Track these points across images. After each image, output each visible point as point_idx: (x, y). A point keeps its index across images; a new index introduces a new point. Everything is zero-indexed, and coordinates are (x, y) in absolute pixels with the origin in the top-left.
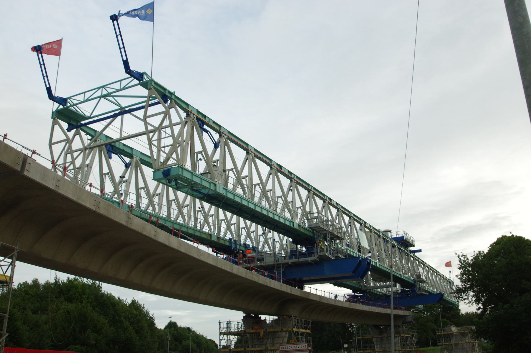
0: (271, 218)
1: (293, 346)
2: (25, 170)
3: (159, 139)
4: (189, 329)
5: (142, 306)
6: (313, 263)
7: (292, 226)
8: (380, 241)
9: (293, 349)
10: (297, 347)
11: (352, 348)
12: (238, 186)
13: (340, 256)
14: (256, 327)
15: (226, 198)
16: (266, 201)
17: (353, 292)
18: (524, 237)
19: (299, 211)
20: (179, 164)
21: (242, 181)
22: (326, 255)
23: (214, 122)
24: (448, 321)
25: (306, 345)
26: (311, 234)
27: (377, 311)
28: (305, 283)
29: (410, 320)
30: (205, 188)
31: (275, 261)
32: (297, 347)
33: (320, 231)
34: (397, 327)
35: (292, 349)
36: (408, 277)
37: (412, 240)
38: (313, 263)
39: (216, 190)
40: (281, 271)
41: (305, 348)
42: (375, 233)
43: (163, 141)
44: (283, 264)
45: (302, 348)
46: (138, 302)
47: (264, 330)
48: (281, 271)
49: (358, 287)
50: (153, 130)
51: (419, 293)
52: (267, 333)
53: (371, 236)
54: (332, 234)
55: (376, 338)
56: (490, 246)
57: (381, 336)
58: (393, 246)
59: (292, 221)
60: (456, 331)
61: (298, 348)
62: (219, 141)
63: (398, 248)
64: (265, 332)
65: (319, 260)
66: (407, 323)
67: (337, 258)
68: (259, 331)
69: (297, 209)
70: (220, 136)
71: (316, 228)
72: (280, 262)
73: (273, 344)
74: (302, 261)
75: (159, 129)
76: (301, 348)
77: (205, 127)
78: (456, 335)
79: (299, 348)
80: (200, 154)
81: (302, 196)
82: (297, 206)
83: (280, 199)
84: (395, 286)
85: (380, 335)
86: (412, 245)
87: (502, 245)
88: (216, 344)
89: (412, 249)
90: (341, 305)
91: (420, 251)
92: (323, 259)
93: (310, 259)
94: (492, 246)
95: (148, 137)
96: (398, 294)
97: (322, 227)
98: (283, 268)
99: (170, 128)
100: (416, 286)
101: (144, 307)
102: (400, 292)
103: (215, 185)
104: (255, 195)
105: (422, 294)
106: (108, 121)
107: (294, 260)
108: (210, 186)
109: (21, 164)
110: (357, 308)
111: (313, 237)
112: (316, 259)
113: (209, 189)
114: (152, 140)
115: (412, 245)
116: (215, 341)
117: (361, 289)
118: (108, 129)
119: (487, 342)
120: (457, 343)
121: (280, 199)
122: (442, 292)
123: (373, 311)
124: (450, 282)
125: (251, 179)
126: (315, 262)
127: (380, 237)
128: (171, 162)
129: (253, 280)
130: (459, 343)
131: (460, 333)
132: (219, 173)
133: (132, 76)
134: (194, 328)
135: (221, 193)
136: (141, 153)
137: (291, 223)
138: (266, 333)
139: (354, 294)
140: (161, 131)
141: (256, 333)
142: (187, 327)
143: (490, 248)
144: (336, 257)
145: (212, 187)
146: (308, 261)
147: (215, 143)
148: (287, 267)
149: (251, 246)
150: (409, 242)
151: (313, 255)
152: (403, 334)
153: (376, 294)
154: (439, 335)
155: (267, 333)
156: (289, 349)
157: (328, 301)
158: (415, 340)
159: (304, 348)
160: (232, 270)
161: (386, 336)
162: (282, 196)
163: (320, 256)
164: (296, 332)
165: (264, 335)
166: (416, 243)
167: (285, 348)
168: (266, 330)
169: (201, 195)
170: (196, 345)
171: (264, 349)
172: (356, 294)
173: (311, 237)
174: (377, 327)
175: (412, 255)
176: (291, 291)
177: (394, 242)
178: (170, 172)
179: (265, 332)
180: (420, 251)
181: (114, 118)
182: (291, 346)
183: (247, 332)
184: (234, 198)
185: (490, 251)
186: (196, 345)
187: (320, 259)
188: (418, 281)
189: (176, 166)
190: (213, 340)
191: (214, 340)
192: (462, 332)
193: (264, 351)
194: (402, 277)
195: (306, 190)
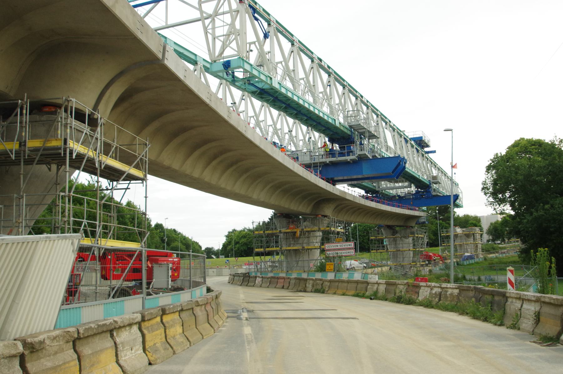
0: (316, 114)
1: (339, 245)
2: (165, 59)
3: (214, 28)
4: (175, 230)
5: (138, 207)
6: (352, 162)
7: (334, 123)
9: (339, 247)
10: (343, 246)
13: (377, 155)
14: (292, 226)
17: (365, 193)
18: (541, 139)
20: (240, 55)
22: (365, 154)
23: (264, 10)
24: (444, 222)
25: (352, 243)
26: (349, 133)
27: (397, 212)
28: (337, 183)
29: (423, 220)
30: (262, 81)
31: (311, 159)
32: (343, 246)
33: (358, 129)
34: (411, 228)
35: (337, 248)
36: (424, 178)
37: (428, 141)
38: (352, 162)
39: (272, 84)
40: (318, 171)
41: (350, 247)
42: (398, 132)
43: (217, 30)
44: (321, 163)
45: (348, 247)
46: (133, 203)
47: (301, 230)
48: (318, 171)
49: (372, 187)
50: (199, 19)
51: (434, 194)
52: (304, 232)
53: (394, 135)
54: (369, 132)
55: (389, 238)
56: (507, 148)
57: (394, 236)
58: (412, 146)
60: (461, 232)
61: (344, 247)
63: (416, 149)
64: (301, 232)
65: (357, 159)
66: (420, 224)
67: (374, 157)
68: (295, 230)
70: (269, 25)
71: (355, 126)
72: (317, 161)
73: (308, 244)
74: (340, 161)
75: (213, 17)
76: (347, 247)
77: (256, 15)
78: (461, 237)
79: (345, 247)
84: (410, 187)
85: (392, 235)
86: (428, 146)
87: (521, 147)
88: (200, 245)
89: (426, 149)
90: (369, 206)
91: (434, 152)
92: (362, 159)
93: (349, 158)
94: (509, 148)
95: (204, 24)
96: (413, 195)
97: (363, 125)
98: (320, 167)
99: (229, 14)
100: (431, 187)
101: (140, 209)
102: (414, 192)
103: (271, 79)
105: (437, 195)
106: (223, 6)
107: (352, 157)
109: (162, 51)
110: (382, 208)
111: (351, 135)
112: (355, 158)
113: (266, 83)
114: (208, 28)
115: (428, 146)
116: (198, 243)
117: (375, 190)
118: (147, 17)
120: (462, 243)
121: (252, 119)
122: (458, 194)
123: (394, 211)
124: (455, 184)
126: (354, 162)
128: (228, 52)
129: (308, 179)
130: (463, 244)
131: (465, 234)
132: (274, 65)
134: (179, 230)
135: (276, 88)
136: (175, 43)
137: (334, 121)
138: (302, 233)
139: (366, 194)
140: (215, 18)
141: (292, 232)
142: (173, 228)
143: (508, 150)
144: (373, 156)
145: (269, 82)
146: (326, 162)
147: (264, 32)
148: (325, 165)
149: (280, 144)
150: (425, 143)
151: (351, 154)
152: (418, 234)
153: (387, 195)
154: (444, 236)
155: (304, 232)
156: (334, 248)
157: (359, 201)
158: (426, 240)
159: (350, 247)
160: (294, 168)
161: (400, 236)
163: (359, 155)
164: (333, 231)
165: (301, 235)
166: (431, 144)
167: (330, 246)
168: (303, 229)
169: (254, 89)
170: (185, 247)
171: (301, 248)
172: (368, 195)
173: (349, 135)
174: (389, 227)
175: (426, 155)
176: (333, 191)
177: (413, 142)
178: (230, 63)
179: (301, 232)
180: (434, 152)
181: (156, 3)
182: (337, 244)
183: (282, 231)
185: (507, 152)
186: (185, 247)
187: (358, 158)
188: (433, 183)
189: (237, 57)
190: (196, 242)
191: (198, 242)
192: (467, 233)
193: (301, 251)
194: (420, 178)
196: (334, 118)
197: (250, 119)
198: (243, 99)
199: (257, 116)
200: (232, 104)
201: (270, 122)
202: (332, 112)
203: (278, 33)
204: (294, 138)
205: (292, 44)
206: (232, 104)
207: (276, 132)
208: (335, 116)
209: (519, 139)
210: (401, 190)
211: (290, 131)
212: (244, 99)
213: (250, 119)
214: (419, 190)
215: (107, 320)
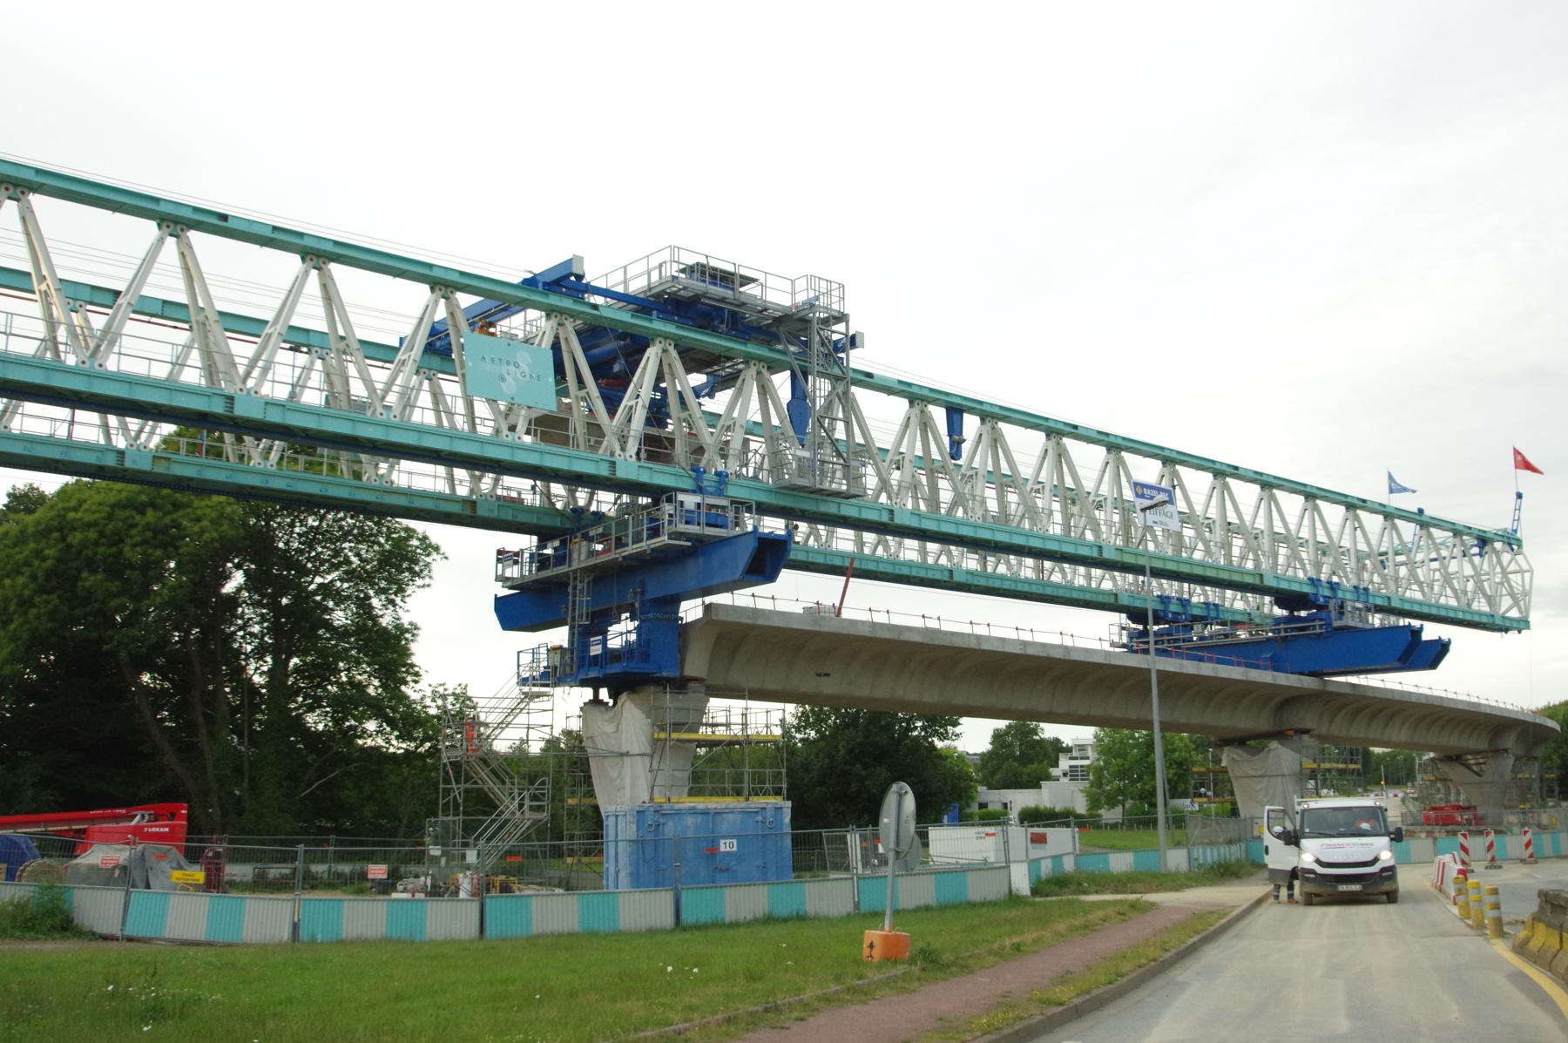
133: (619, 300)
137: (1258, 577)
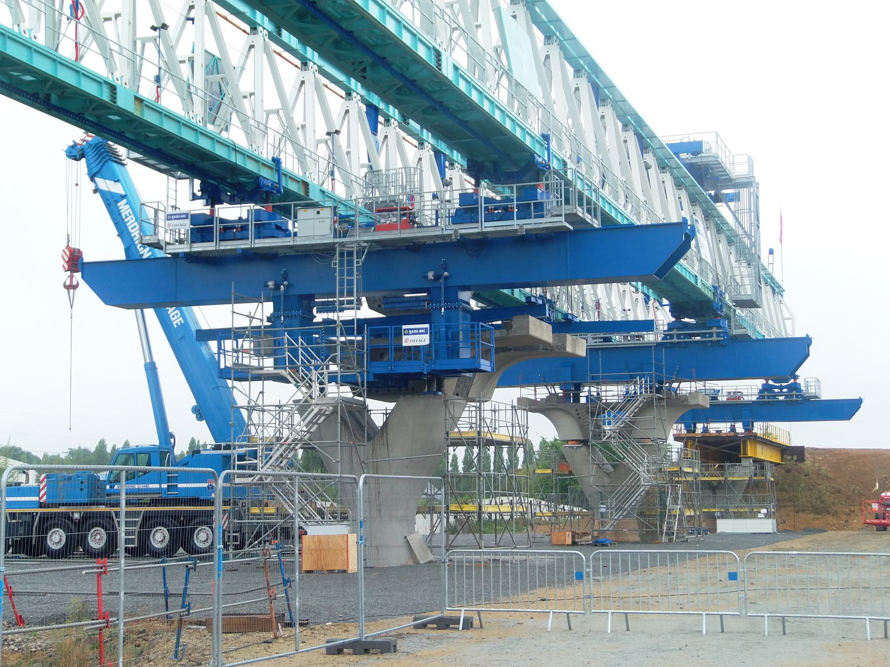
8: (386, 137)
11: (774, 512)
12: (90, 45)
15: (54, 82)
16: (295, 156)
19: (274, 122)
21: (103, 28)
59: (106, 82)
62: (252, 44)
69: (268, 116)
80: (152, 43)
81: (226, 42)
82: (268, 106)
83: (273, 118)
104: (142, 74)
108: (101, 91)
119: (91, 608)
121: (273, 118)
125: (133, 24)
127: (255, 29)
137: (433, 57)
160: (176, 182)
162: (281, 109)
184: (79, 83)
195: (287, 51)
196: (437, 47)
197: (144, 45)
198: (188, 19)
199: (286, 109)
200: (154, 28)
201: (272, 101)
202: (429, 23)
203: (534, 25)
204: (300, 132)
205: (575, 71)
206: (154, 28)
207: (289, 134)
208: (438, 41)
209: (97, 444)
210: (589, 391)
211: (333, 133)
212: (193, 20)
213: (144, 45)
214: (770, 382)
215: (570, 447)
